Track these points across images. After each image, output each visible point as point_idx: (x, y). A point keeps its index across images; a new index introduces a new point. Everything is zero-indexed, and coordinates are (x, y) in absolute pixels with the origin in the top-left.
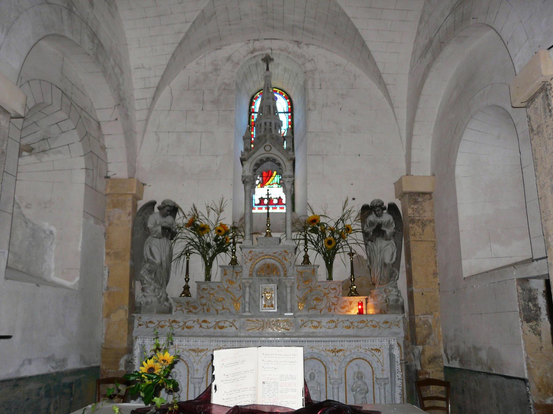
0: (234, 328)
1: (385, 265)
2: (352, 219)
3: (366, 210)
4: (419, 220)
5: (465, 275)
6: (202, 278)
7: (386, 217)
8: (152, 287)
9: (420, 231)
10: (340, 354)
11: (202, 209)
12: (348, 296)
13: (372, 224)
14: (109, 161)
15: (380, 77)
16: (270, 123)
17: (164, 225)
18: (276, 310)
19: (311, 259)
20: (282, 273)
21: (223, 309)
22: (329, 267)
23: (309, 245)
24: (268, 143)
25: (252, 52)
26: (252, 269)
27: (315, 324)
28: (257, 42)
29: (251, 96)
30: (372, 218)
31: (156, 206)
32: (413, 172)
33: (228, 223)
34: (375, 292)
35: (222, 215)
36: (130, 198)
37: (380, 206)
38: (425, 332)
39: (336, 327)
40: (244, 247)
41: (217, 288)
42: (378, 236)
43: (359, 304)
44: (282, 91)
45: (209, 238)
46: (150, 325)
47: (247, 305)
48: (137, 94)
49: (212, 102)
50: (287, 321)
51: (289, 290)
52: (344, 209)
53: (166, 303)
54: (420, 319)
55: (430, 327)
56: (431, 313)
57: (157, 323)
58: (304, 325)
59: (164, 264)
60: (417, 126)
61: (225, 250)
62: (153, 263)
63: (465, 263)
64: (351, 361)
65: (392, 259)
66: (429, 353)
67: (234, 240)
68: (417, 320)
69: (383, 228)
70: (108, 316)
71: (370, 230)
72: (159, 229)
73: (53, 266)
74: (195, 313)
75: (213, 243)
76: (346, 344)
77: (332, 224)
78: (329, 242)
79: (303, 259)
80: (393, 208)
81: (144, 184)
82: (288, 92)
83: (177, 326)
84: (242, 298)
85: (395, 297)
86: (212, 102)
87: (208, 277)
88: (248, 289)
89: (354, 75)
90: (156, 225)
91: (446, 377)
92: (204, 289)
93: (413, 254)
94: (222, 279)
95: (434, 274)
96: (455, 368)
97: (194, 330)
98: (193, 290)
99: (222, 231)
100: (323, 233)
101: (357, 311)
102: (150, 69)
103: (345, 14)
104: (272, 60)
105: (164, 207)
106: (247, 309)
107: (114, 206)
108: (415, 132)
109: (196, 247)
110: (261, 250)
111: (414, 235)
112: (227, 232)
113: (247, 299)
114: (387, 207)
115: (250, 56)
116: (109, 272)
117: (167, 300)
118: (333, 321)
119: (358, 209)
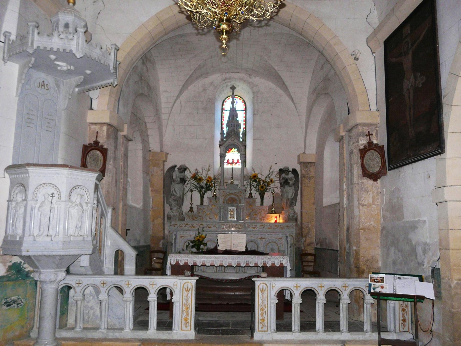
0: (215, 228)
1: (288, 199)
2: (274, 176)
3: (281, 171)
4: (307, 176)
5: (324, 205)
6: (199, 203)
7: (291, 175)
8: (176, 208)
9: (308, 181)
10: (264, 240)
11: (200, 170)
12: (271, 213)
13: (283, 178)
14: (150, 142)
15: (292, 99)
16: (234, 125)
17: (181, 177)
18: (235, 220)
19: (253, 195)
20: (239, 202)
21: (210, 218)
22: (262, 199)
23: (253, 188)
24: (233, 137)
25: (224, 80)
26: (224, 200)
27: (254, 226)
28: (227, 74)
29: (223, 101)
30: (284, 175)
31: (176, 169)
32: (306, 152)
33: (212, 176)
34: (283, 212)
35: (209, 172)
36: (162, 162)
37: (287, 170)
38: (307, 231)
39: (263, 228)
40: (221, 189)
41: (207, 209)
42: (286, 185)
43: (275, 218)
44: (241, 97)
45: (203, 183)
46: (175, 226)
47: (222, 217)
48: (163, 105)
49: (203, 109)
50: (241, 225)
51: (241, 210)
52: (270, 171)
53: (182, 216)
54: (305, 225)
55: (309, 229)
56: (310, 223)
57: (179, 225)
58: (249, 227)
59: (181, 197)
60: (309, 127)
61: (211, 190)
62: (176, 196)
63: (325, 200)
64: (269, 243)
65: (292, 196)
66: (308, 241)
67: (215, 185)
68: (303, 225)
69: (289, 181)
70: (153, 221)
71: (283, 181)
72: (179, 179)
73: (130, 198)
74: (196, 221)
75: (205, 186)
76: (267, 236)
77: (263, 178)
78: (262, 187)
79: (249, 195)
80: (294, 171)
81: (168, 154)
82: (244, 99)
83: (188, 226)
84: (219, 214)
85: (293, 215)
86: (203, 109)
87: (202, 203)
88: (222, 209)
89: (280, 95)
90: (177, 177)
91: (315, 252)
92: (200, 209)
93: (304, 194)
94: (209, 204)
95: (313, 203)
96: (318, 248)
97: (183, 227)
98: (195, 209)
99: (209, 180)
100: (259, 181)
101: (274, 221)
102: (171, 92)
103: (274, 69)
104: (235, 88)
105: (181, 169)
106: (222, 219)
107: (154, 166)
108: (308, 131)
109: (196, 187)
110: (228, 191)
111: (305, 184)
112: (212, 181)
113: (222, 214)
114: (291, 171)
115: (224, 82)
116: (152, 200)
117: (182, 214)
118: (263, 226)
119: (277, 170)
